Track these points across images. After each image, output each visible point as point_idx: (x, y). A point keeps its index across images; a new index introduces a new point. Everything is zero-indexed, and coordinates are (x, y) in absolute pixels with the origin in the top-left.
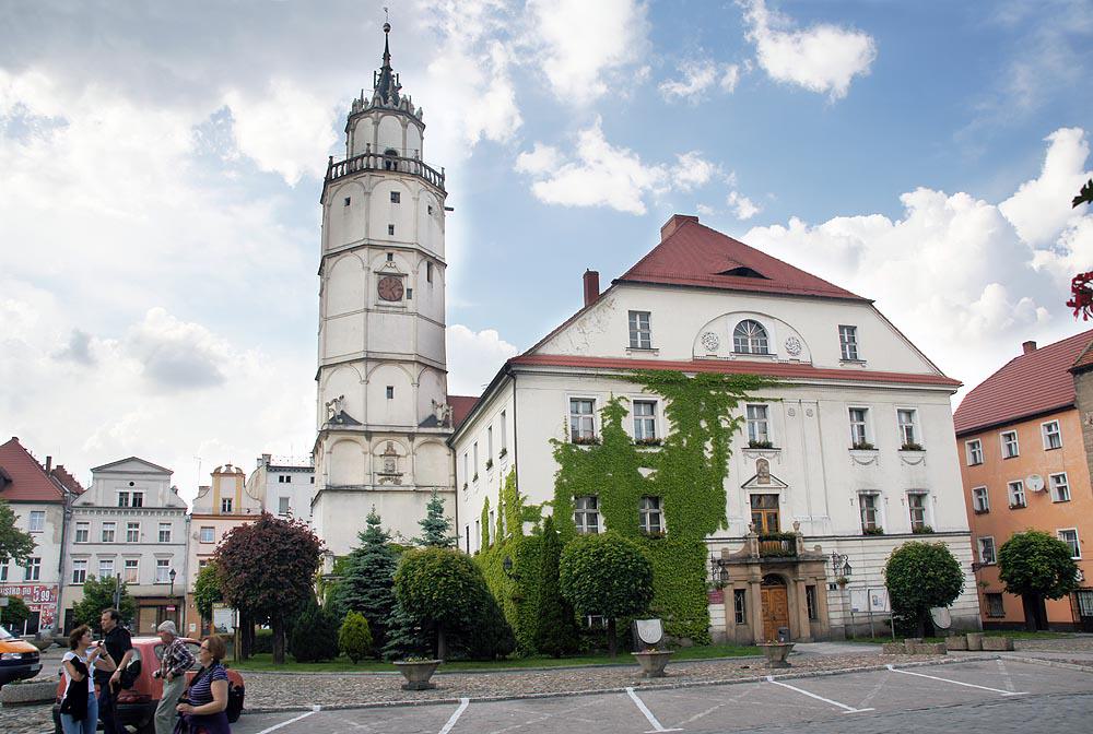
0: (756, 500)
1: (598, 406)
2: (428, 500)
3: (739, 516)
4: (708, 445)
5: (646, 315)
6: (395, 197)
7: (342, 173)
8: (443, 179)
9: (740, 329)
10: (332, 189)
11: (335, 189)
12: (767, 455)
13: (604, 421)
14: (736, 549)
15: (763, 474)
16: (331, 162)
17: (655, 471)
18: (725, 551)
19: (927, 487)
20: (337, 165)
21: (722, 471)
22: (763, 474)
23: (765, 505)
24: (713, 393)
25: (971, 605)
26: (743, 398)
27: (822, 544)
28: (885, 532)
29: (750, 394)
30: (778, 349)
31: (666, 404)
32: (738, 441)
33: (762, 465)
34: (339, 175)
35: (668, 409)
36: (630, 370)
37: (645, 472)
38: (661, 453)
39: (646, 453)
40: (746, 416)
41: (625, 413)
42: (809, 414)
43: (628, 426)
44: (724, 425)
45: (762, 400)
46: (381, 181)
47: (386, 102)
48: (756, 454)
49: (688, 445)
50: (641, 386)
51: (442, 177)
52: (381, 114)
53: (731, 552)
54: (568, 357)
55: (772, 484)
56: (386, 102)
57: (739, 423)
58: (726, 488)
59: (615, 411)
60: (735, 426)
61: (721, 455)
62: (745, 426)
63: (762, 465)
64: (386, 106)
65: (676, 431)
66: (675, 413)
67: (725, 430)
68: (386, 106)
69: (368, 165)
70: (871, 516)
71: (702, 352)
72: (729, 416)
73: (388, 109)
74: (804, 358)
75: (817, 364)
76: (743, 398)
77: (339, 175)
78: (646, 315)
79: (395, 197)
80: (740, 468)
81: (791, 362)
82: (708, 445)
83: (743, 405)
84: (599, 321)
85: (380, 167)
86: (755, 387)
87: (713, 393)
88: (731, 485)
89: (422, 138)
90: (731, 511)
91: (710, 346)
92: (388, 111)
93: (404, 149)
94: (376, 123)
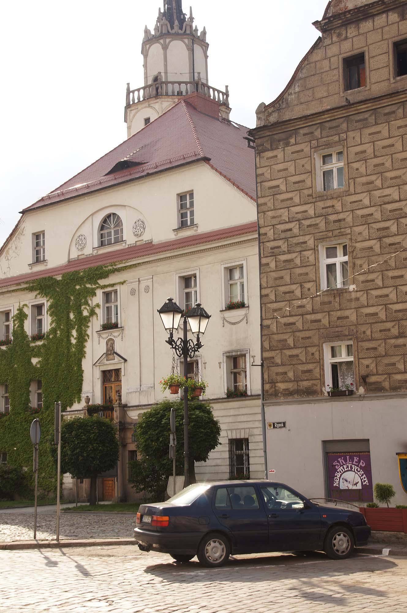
1: (12, 315)
4: (74, 333)
7: (139, 98)
8: (227, 96)
10: (131, 114)
11: (133, 112)
12: (115, 333)
13: (14, 326)
15: (111, 352)
16: (128, 89)
17: (40, 359)
20: (133, 92)
21: (81, 353)
22: (111, 352)
24: (78, 287)
26: (98, 287)
28: (249, 393)
29: (102, 282)
31: (49, 304)
32: (96, 323)
33: (110, 344)
34: (136, 101)
35: (51, 307)
36: (27, 283)
37: (34, 361)
38: (44, 345)
39: (36, 346)
40: (101, 304)
41: (26, 316)
42: (147, 289)
43: (29, 328)
44: (85, 313)
45: (113, 285)
46: (136, 113)
47: (172, 28)
48: (106, 335)
49: (61, 334)
50: (35, 293)
51: (227, 94)
52: (168, 40)
54: (17, 277)
56: (172, 28)
57: (97, 310)
58: (84, 368)
59: (21, 316)
60: (92, 313)
61: (82, 339)
62: (100, 312)
63: (110, 344)
64: (173, 31)
65: (53, 325)
66: (55, 310)
67: (86, 317)
68: (173, 31)
70: (235, 381)
71: (74, 255)
72: (89, 306)
73: (177, 34)
74: (146, 238)
75: (156, 241)
76: (98, 287)
77: (136, 101)
80: (95, 347)
81: (138, 243)
82: (74, 333)
83: (99, 293)
84: (16, 248)
86: (105, 275)
87: (78, 287)
88: (87, 365)
89: (206, 57)
90: (86, 388)
91: (80, 247)
92: (176, 36)
93: (166, 73)
94: (165, 48)
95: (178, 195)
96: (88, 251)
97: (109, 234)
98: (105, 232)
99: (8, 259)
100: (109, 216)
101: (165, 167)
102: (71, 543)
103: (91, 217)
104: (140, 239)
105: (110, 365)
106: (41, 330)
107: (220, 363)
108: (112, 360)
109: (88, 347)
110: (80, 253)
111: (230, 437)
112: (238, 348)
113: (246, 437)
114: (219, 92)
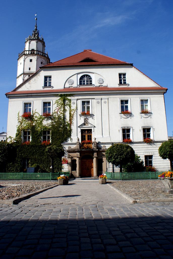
0: (83, 131)
2: (78, 128)
3: (76, 136)
5: (124, 75)
6: (31, 61)
9: (82, 78)
14: (73, 147)
18: (69, 147)
19: (151, 126)
23: (86, 133)
25: (167, 167)
27: (106, 145)
30: (95, 82)
53: (72, 148)
55: (89, 126)
63: (86, 120)
68: (32, 38)
69: (26, 53)
71: (67, 86)
74: (104, 85)
75: (109, 86)
78: (124, 75)
79: (31, 61)
85: (30, 53)
88: (74, 127)
95: (51, 76)
96: (75, 85)
97: (84, 81)
98: (82, 80)
99: (30, 84)
100: (84, 76)
101: (71, 65)
102: (45, 189)
103: (76, 75)
104: (101, 85)
105: (85, 127)
106: (89, 111)
107: (119, 130)
108: (87, 125)
109: (74, 121)
110: (70, 86)
111: (145, 155)
112: (148, 125)
113: (152, 155)
114: (40, 52)
